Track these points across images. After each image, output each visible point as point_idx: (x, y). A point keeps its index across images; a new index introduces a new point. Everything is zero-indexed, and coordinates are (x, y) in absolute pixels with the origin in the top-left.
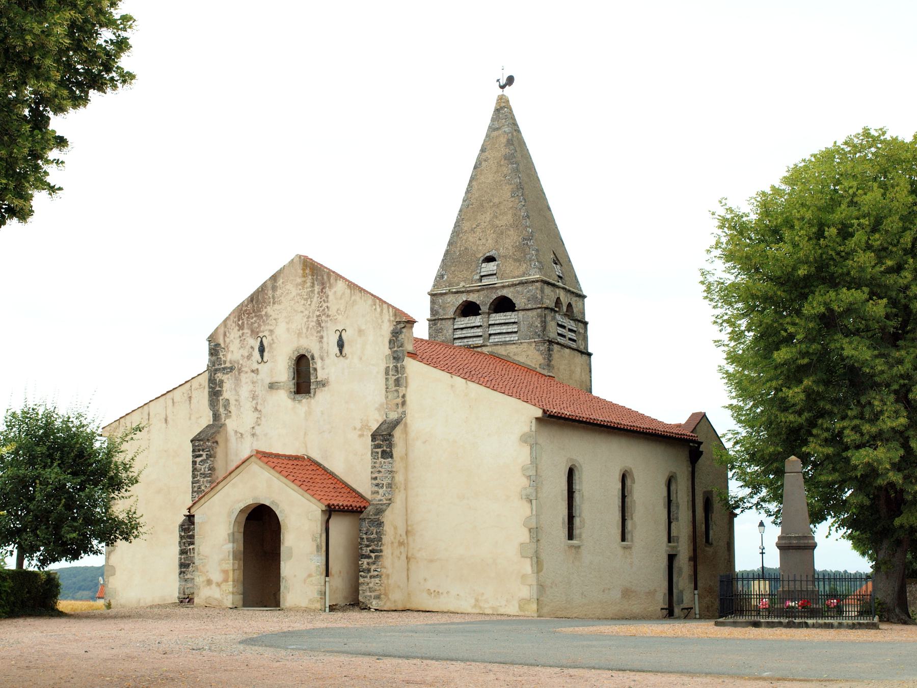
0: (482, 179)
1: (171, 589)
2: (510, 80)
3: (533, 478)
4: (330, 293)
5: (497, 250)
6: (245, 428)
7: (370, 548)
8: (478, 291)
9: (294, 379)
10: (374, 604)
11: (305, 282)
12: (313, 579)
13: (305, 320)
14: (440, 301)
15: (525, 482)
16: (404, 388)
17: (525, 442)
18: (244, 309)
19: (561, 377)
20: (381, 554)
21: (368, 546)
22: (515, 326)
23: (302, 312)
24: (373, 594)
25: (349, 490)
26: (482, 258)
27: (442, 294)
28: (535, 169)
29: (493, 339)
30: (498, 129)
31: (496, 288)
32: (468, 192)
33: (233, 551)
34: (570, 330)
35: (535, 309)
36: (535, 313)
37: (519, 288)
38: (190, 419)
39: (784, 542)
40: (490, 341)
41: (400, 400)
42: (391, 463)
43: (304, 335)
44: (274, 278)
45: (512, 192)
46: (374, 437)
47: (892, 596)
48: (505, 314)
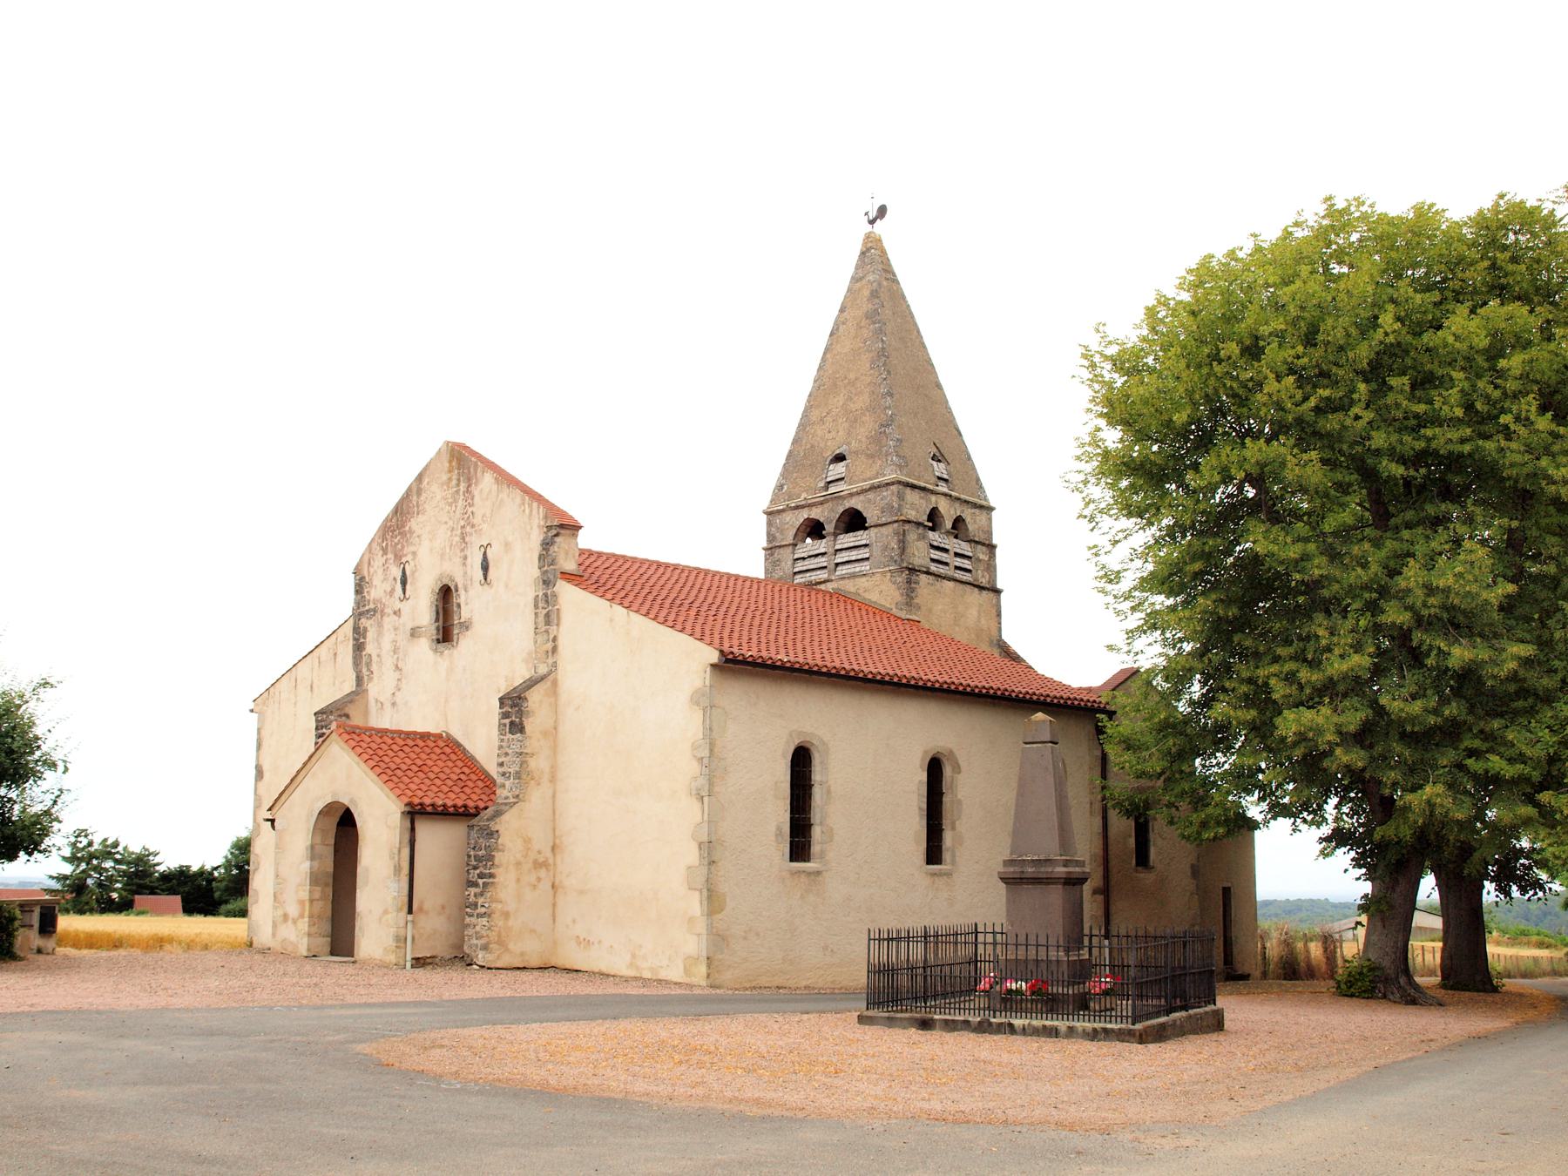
1: (1056, 895)
2: (882, 211)
3: (706, 761)
4: (476, 493)
5: (849, 444)
6: (385, 697)
7: (478, 871)
8: (821, 503)
9: (437, 620)
10: (481, 957)
11: (450, 479)
12: (389, 916)
13: (449, 533)
15: (695, 767)
16: (555, 627)
17: (698, 704)
18: (389, 524)
19: (936, 621)
20: (491, 880)
21: (475, 868)
22: (867, 550)
23: (446, 523)
24: (479, 942)
27: (779, 512)
28: (918, 332)
29: (842, 571)
30: (861, 279)
31: (843, 498)
32: (820, 368)
33: (311, 873)
35: (890, 523)
36: (890, 529)
37: (871, 495)
38: (334, 684)
39: (1012, 869)
40: (837, 573)
41: (549, 646)
42: (521, 741)
43: (447, 556)
44: (420, 478)
45: (873, 362)
46: (502, 700)
47: (1393, 956)
48: (855, 534)
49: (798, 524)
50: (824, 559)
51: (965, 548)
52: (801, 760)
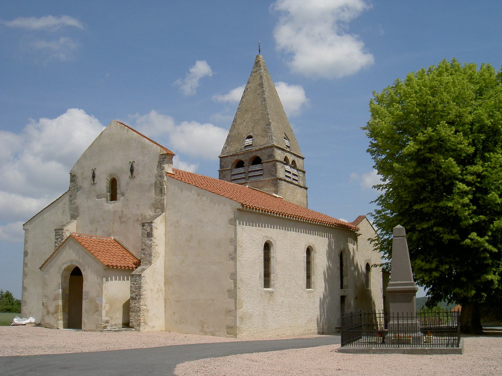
0: (247, 97)
14: (225, 160)
25: (134, 257)
26: (246, 137)
27: (225, 157)
31: (252, 152)
34: (293, 174)
49: (233, 161)
50: (261, 172)
51: (295, 172)
52: (267, 246)
